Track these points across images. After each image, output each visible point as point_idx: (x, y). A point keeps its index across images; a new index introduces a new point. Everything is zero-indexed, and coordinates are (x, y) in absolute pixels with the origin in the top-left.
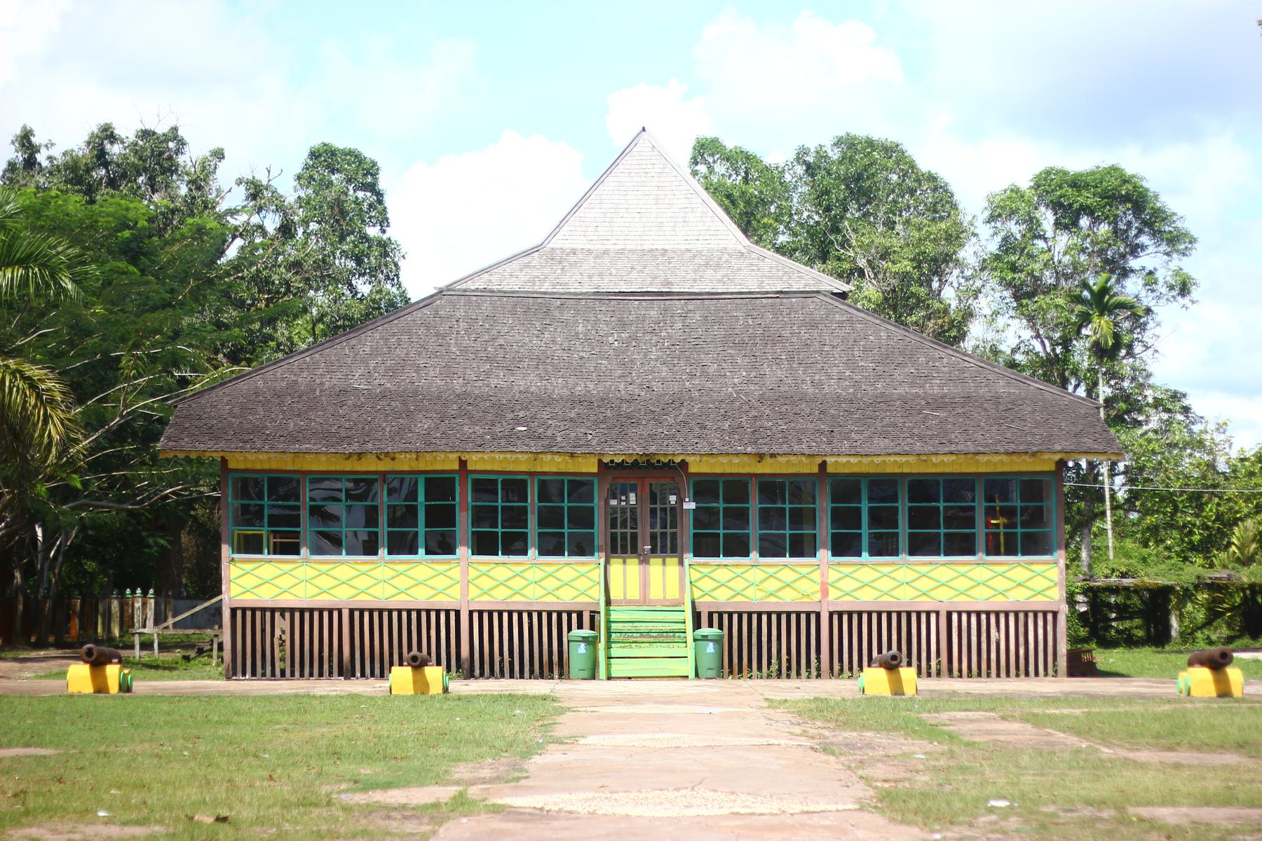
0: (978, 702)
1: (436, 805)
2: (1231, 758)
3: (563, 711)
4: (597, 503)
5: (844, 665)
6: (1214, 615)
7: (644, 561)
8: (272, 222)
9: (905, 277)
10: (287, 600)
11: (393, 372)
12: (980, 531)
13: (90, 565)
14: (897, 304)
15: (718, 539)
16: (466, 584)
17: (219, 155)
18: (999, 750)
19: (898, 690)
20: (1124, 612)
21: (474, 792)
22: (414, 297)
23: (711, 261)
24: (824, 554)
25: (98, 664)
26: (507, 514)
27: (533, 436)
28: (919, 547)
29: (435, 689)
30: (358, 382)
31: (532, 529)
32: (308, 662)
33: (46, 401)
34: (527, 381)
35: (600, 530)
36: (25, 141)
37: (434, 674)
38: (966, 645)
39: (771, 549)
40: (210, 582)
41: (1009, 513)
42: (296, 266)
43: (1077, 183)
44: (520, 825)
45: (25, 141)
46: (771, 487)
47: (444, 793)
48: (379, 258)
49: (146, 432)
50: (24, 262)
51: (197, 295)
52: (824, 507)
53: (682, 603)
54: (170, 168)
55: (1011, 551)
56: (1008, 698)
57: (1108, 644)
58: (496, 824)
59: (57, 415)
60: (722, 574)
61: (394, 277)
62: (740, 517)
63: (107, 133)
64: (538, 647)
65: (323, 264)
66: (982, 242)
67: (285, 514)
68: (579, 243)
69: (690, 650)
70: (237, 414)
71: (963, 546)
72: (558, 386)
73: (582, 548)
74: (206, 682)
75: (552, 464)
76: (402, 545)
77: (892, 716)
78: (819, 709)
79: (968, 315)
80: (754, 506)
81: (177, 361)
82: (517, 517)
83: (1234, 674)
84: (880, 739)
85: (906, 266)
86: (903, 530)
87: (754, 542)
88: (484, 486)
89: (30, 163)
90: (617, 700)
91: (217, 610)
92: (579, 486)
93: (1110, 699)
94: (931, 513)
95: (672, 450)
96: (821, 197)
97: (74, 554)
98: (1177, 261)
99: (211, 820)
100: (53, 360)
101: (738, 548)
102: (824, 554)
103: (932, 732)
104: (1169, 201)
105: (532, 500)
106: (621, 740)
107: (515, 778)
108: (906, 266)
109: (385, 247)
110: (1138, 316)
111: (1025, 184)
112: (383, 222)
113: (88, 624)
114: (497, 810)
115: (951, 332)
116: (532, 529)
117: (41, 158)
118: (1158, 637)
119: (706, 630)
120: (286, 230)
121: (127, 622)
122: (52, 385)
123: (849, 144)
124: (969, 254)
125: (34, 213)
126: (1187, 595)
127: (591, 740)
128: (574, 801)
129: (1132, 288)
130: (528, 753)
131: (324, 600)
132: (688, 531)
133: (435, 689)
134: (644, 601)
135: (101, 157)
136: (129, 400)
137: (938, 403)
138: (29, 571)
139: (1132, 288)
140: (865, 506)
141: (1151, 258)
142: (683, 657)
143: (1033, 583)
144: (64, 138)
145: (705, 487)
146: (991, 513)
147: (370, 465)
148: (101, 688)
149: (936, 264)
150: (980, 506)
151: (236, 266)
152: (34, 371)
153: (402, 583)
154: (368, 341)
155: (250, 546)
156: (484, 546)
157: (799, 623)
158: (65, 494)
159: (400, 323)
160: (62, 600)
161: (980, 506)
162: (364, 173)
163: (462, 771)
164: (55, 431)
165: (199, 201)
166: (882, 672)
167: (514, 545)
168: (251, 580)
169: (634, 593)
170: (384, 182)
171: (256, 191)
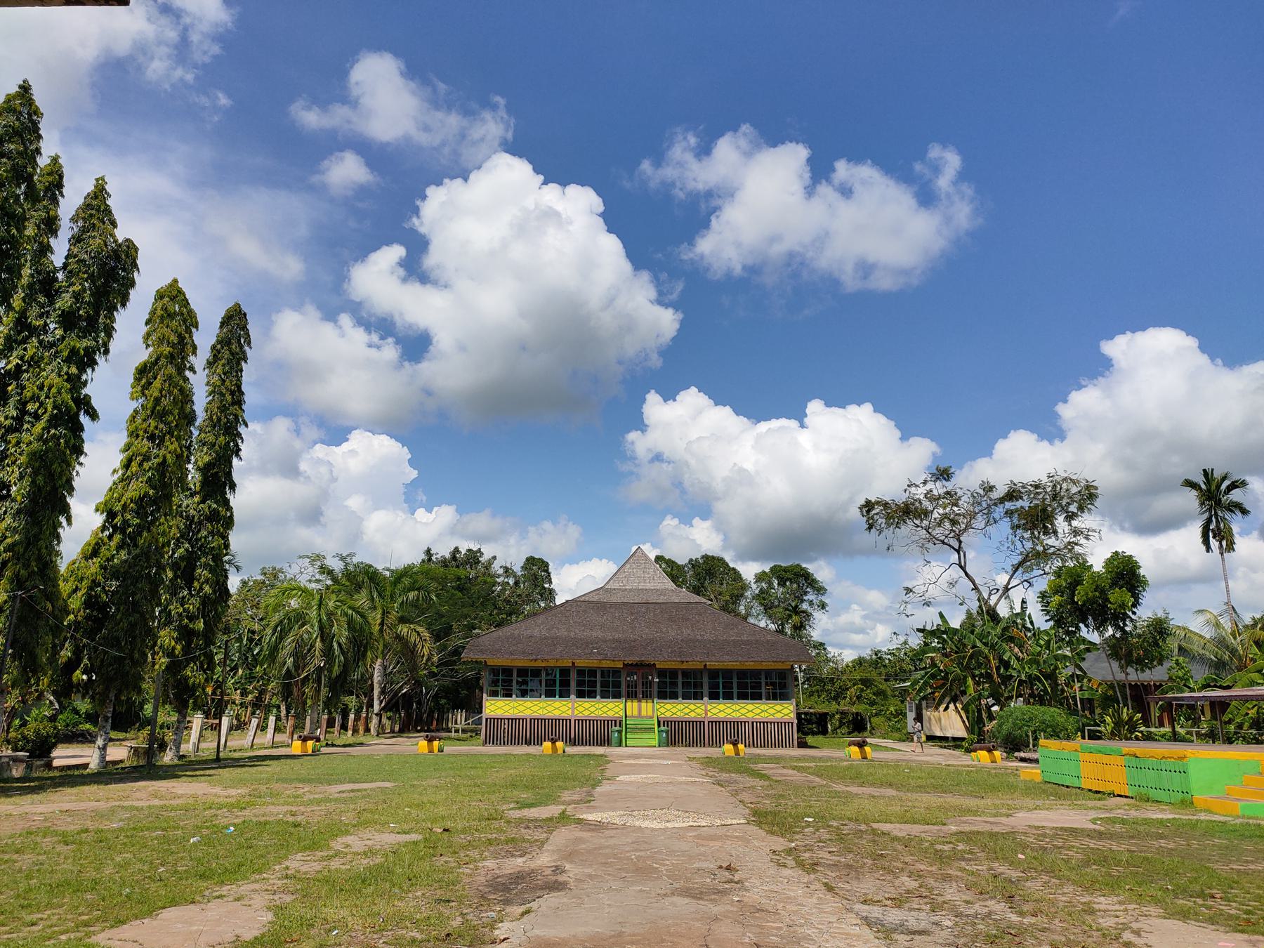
0: (776, 759)
1: (551, 819)
3: (609, 762)
4: (623, 679)
5: (716, 742)
6: (841, 724)
7: (639, 701)
8: (511, 581)
9: (726, 601)
10: (507, 715)
12: (763, 691)
13: (443, 701)
15: (667, 693)
16: (573, 709)
17: (495, 558)
19: (737, 753)
24: (706, 699)
25: (430, 740)
26: (590, 683)
27: (599, 653)
29: (560, 751)
31: (598, 688)
33: (423, 640)
34: (597, 634)
35: (623, 689)
37: (560, 744)
38: (760, 734)
39: (686, 697)
41: (772, 684)
43: (786, 570)
44: (589, 834)
46: (686, 673)
47: (553, 810)
49: (457, 652)
50: (418, 589)
52: (706, 680)
53: (652, 717)
55: (775, 698)
59: (427, 645)
60: (668, 706)
62: (674, 684)
63: (457, 550)
64: (603, 733)
65: (528, 595)
67: (516, 680)
68: (617, 586)
69: (657, 737)
70: (491, 645)
71: (756, 697)
72: (609, 635)
73: (617, 696)
74: (475, 748)
76: (550, 694)
78: (708, 762)
80: (680, 680)
82: (593, 684)
85: (727, 598)
87: (680, 694)
88: (581, 672)
89: (430, 560)
90: (630, 757)
92: (616, 672)
94: (747, 684)
95: (650, 659)
96: (697, 575)
97: (436, 697)
99: (440, 831)
101: (674, 696)
106: (633, 778)
107: (587, 801)
108: (727, 598)
109: (551, 591)
110: (808, 616)
112: (550, 582)
113: (440, 721)
114: (580, 821)
116: (598, 688)
117: (433, 558)
119: (662, 728)
120: (517, 583)
122: (426, 634)
123: (706, 557)
124: (748, 594)
127: (621, 778)
129: (805, 606)
130: (594, 786)
131: (521, 715)
132: (655, 689)
133: (560, 751)
134: (639, 716)
137: (748, 643)
138: (419, 703)
140: (721, 681)
143: (783, 711)
145: (662, 673)
146: (767, 684)
147: (540, 664)
148: (431, 751)
150: (763, 681)
155: (494, 694)
156: (581, 694)
158: (433, 675)
161: (763, 681)
162: (544, 565)
163: (566, 796)
164: (426, 651)
166: (856, 749)
167: (592, 695)
168: (495, 707)
170: (551, 569)
171: (507, 570)
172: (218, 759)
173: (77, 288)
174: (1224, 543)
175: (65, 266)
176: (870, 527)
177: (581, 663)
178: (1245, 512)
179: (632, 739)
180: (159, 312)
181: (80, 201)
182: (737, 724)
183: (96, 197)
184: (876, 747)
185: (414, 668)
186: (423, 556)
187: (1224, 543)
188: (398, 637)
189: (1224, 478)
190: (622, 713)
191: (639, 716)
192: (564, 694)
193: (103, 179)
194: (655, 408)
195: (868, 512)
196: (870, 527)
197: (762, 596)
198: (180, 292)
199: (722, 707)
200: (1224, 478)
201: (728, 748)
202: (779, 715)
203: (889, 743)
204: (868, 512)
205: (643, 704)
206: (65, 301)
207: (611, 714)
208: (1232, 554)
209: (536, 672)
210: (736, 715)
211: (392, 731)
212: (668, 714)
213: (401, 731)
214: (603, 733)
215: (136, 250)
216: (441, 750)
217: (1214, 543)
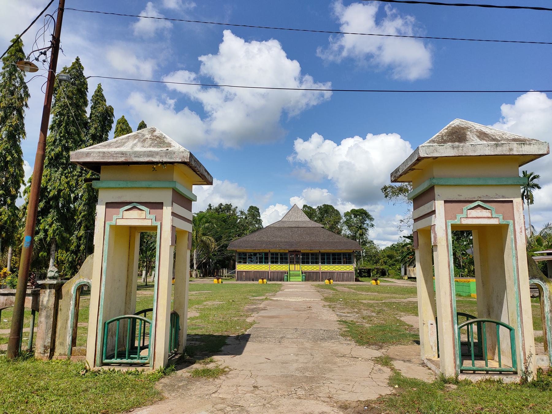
2: (376, 294)
5: (323, 280)
6: (377, 273)
8: (244, 217)
10: (245, 270)
11: (260, 238)
14: (332, 228)
15: (305, 261)
16: (270, 268)
17: (237, 207)
18: (343, 292)
19: (330, 283)
20: (364, 272)
21: (268, 297)
22: (264, 227)
23: (304, 222)
24: (320, 264)
25: (218, 279)
26: (277, 258)
28: (334, 263)
30: (255, 239)
32: (248, 279)
34: (279, 239)
35: (289, 260)
36: (210, 205)
37: (265, 280)
38: (341, 277)
39: (312, 263)
40: (234, 268)
41: (346, 258)
42: (247, 223)
43: (357, 211)
45: (210, 205)
46: (312, 254)
47: (264, 297)
48: (259, 222)
49: (226, 246)
50: (209, 223)
51: (233, 227)
52: (320, 257)
54: (230, 209)
56: (346, 285)
57: (362, 277)
58: (271, 302)
59: (213, 244)
60: (306, 267)
61: (261, 224)
63: (221, 204)
64: (281, 277)
66: (344, 219)
67: (245, 258)
70: (237, 244)
71: (340, 263)
72: (283, 240)
74: (234, 282)
75: (282, 251)
76: (261, 262)
77: (329, 287)
78: (319, 286)
79: (342, 230)
80: (310, 257)
81: (230, 237)
83: (378, 281)
84: (327, 290)
85: (333, 223)
86: (331, 261)
88: (272, 254)
89: (210, 209)
91: (235, 272)
92: (285, 254)
93: (360, 285)
95: (299, 249)
96: (321, 213)
97: (216, 263)
98: (371, 222)
100: (213, 236)
101: (308, 263)
102: (320, 264)
103: (334, 289)
104: (370, 213)
105: (279, 256)
107: (274, 295)
108: (333, 223)
109: (260, 220)
110: (366, 230)
111: (349, 211)
112: (260, 216)
113: (217, 273)
114: (271, 300)
115: (339, 233)
118: (369, 276)
120: (246, 218)
121: (223, 273)
122: (213, 240)
123: (325, 205)
124: (341, 221)
125: (211, 216)
126: (373, 270)
128: (282, 299)
129: (365, 226)
132: (301, 261)
134: (295, 270)
135: (220, 208)
136: (223, 242)
137: (336, 243)
139: (365, 226)
141: (368, 222)
142: (300, 278)
143: (350, 268)
144: (215, 205)
145: (303, 254)
148: (218, 283)
149: (337, 222)
151: (239, 223)
152: (210, 238)
153: (261, 268)
154: (256, 233)
155: (240, 262)
157: (317, 273)
158: (214, 255)
159: (262, 231)
160: (214, 270)
162: (257, 210)
163: (267, 294)
164: (213, 246)
165: (234, 214)
166: (374, 281)
168: (240, 267)
169: (293, 269)
171: (242, 213)
172: (146, 285)
173: (96, 126)
174: (529, 201)
175: (90, 118)
176: (386, 197)
177: (272, 251)
178: (539, 188)
179: (292, 279)
180: (119, 129)
181: (93, 93)
182: (332, 273)
183: (99, 92)
184: (381, 281)
185: (209, 252)
186: (208, 207)
187: (529, 201)
188: (202, 241)
189: (531, 175)
190: (288, 269)
191: (295, 270)
192: (266, 262)
193: (100, 84)
194: (300, 145)
195: (385, 191)
196: (386, 197)
197: (347, 223)
198: (126, 121)
199: (326, 267)
200: (531, 175)
201: (327, 282)
202: (348, 270)
203: (393, 280)
204: (385, 191)
205: (296, 266)
206: (92, 131)
207: (284, 269)
208: (532, 205)
209: (255, 254)
210: (331, 270)
211: (200, 276)
212: (306, 270)
213: (203, 276)
214: (281, 277)
215: (113, 109)
216: (222, 283)
217: (526, 201)
